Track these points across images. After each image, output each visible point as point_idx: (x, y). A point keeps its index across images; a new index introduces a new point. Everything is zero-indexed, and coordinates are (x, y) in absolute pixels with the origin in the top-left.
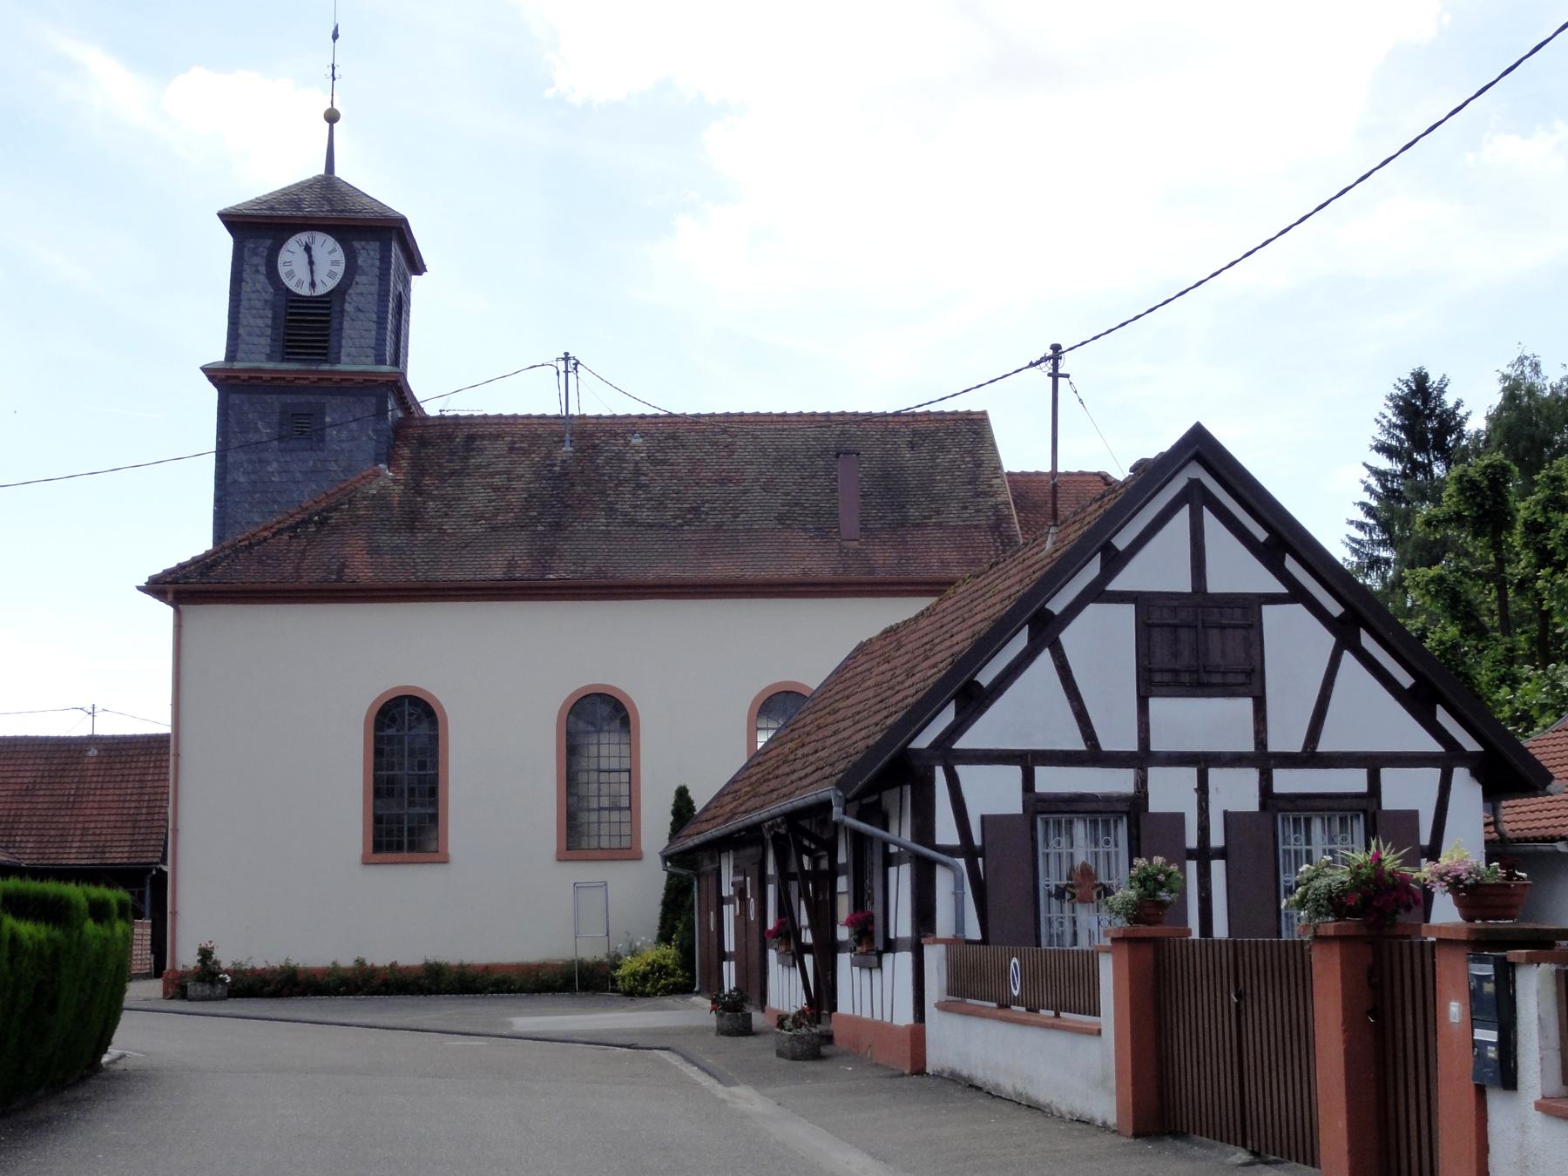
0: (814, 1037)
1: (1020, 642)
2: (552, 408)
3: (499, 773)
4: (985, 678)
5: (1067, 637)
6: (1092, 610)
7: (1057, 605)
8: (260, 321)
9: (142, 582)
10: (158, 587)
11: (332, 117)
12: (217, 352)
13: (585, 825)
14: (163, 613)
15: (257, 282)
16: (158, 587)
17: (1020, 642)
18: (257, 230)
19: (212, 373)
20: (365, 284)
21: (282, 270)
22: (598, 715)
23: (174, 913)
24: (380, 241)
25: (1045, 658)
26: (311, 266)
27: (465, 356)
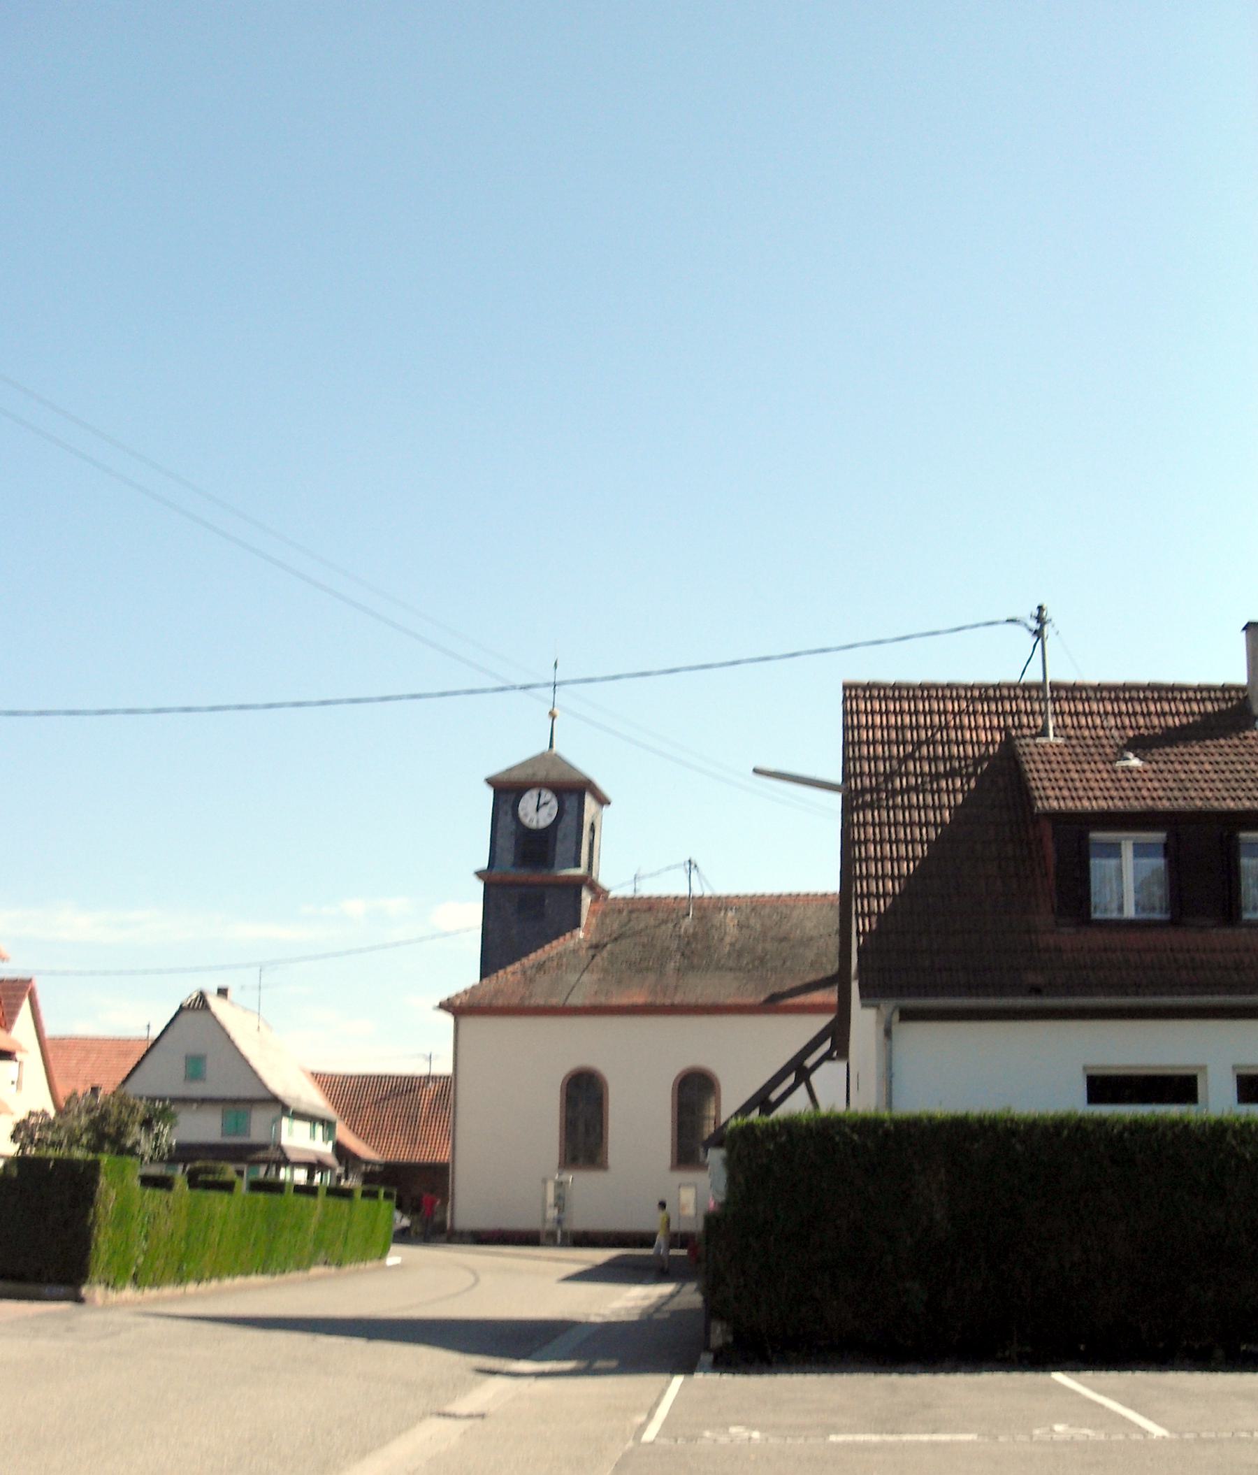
0: (153, 1100)
1: (791, 1079)
2: (683, 892)
3: (640, 1119)
4: (774, 1096)
5: (814, 1078)
6: (826, 1066)
7: (809, 1063)
8: (507, 843)
9: (437, 1004)
10: (446, 1006)
11: (553, 716)
12: (484, 863)
13: (686, 1154)
14: (448, 1020)
15: (506, 820)
16: (446, 1006)
17: (791, 1079)
18: (506, 791)
19: (480, 874)
20: (569, 820)
21: (521, 813)
22: (694, 1089)
23: (453, 1194)
24: (574, 792)
25: (802, 1088)
26: (537, 812)
27: (630, 858)
